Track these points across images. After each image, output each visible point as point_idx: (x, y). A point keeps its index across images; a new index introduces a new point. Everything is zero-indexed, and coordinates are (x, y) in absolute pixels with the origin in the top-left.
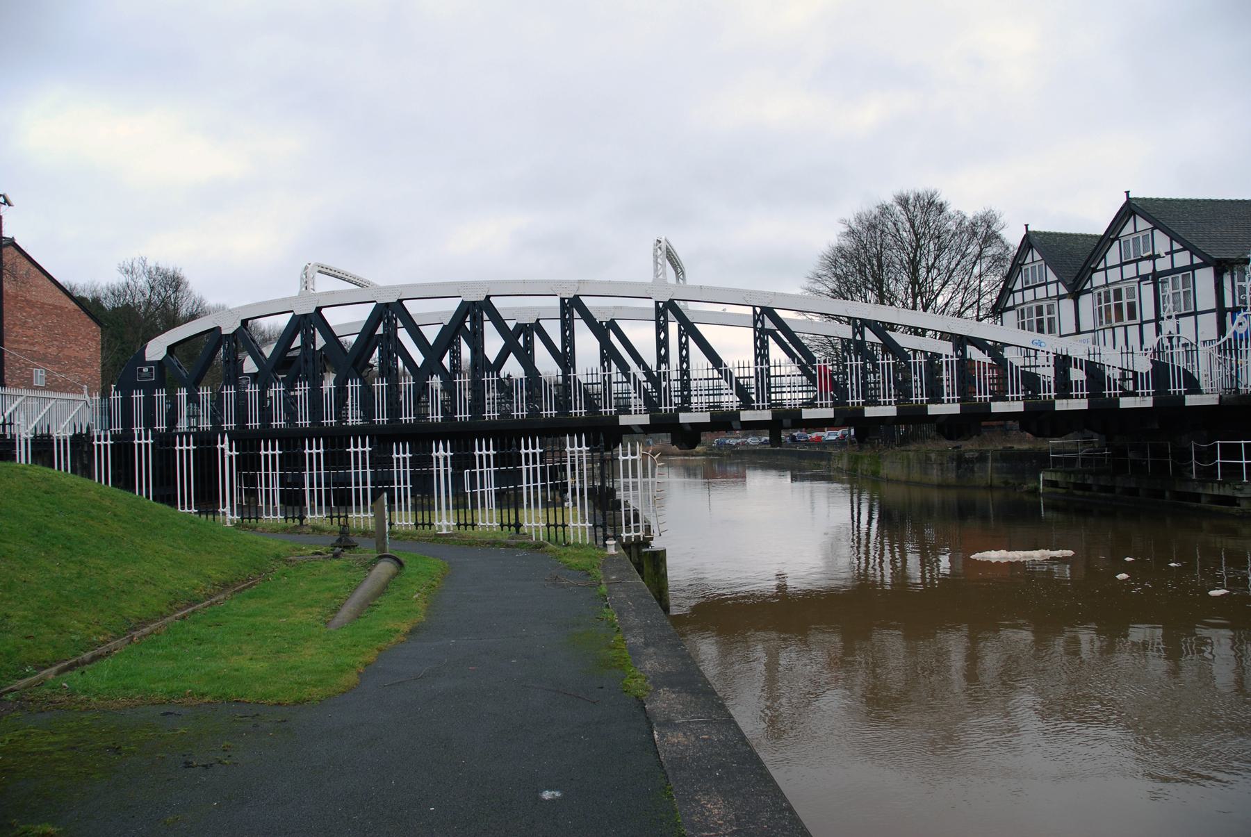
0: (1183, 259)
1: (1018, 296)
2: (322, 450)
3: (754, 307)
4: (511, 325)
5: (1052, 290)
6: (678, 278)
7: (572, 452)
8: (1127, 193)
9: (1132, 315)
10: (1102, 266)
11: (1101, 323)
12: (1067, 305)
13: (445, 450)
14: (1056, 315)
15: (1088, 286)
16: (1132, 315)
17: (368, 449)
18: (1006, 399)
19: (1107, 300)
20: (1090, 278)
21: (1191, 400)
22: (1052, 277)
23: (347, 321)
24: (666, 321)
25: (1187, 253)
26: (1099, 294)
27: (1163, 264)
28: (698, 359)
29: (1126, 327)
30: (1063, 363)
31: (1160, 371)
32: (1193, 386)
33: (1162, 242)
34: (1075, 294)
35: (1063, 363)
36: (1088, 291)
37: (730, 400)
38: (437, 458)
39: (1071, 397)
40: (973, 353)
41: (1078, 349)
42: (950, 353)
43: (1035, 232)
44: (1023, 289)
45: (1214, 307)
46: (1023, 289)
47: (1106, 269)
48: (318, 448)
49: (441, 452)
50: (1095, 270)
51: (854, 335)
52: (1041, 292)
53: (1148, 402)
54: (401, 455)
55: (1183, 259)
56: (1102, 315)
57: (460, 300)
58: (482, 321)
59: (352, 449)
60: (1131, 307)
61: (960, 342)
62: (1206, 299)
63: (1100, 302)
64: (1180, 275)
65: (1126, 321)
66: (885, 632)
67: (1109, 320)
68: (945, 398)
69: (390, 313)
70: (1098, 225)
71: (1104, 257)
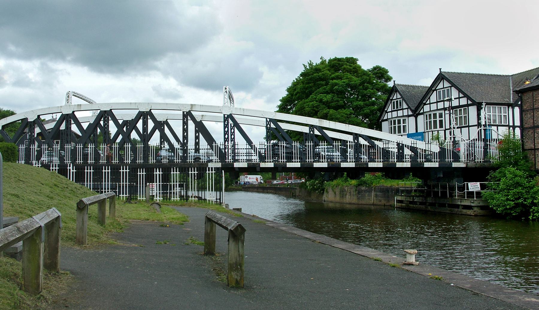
0: (463, 101)
1: (390, 114)
2: (110, 171)
3: (266, 118)
4: (120, 122)
5: (405, 113)
6: (231, 102)
7: (123, 197)
8: (440, 69)
9: (441, 126)
10: (428, 102)
11: (427, 129)
12: (412, 119)
13: (159, 172)
14: (407, 124)
15: (422, 111)
16: (441, 126)
17: (128, 171)
18: (375, 162)
19: (395, 124)
20: (423, 107)
21: (455, 165)
22: (405, 106)
23: (86, 117)
24: (187, 120)
25: (465, 99)
26: (427, 116)
27: (455, 103)
28: (203, 143)
29: (438, 131)
30: (400, 147)
31: (442, 152)
32: (456, 158)
33: (455, 93)
34: (416, 114)
35: (400, 147)
36: (422, 114)
37: (255, 158)
38: (156, 175)
39: (403, 162)
40: (362, 141)
41: (407, 141)
42: (352, 140)
43: (398, 85)
44: (392, 111)
45: (476, 124)
46: (392, 111)
47: (430, 104)
48: (108, 169)
49: (158, 172)
50: (425, 104)
51: (310, 131)
52: (400, 113)
53: (436, 165)
54: (141, 173)
55: (463, 101)
56: (428, 125)
57: (138, 111)
58: (109, 120)
59: (122, 171)
60: (441, 122)
61: (356, 136)
62: (473, 120)
63: (391, 125)
64: (462, 109)
65: (438, 128)
66: (338, 205)
67: (430, 128)
68: (349, 160)
69: (106, 115)
70: (428, 83)
71: (429, 98)
